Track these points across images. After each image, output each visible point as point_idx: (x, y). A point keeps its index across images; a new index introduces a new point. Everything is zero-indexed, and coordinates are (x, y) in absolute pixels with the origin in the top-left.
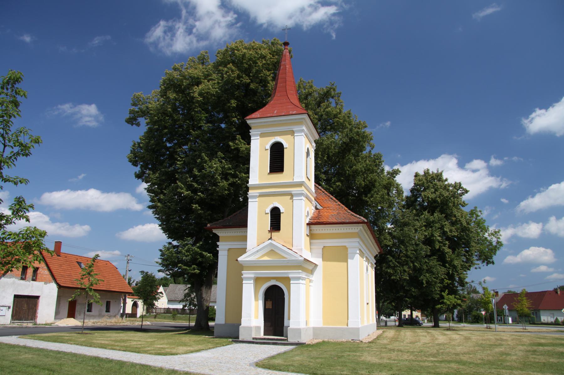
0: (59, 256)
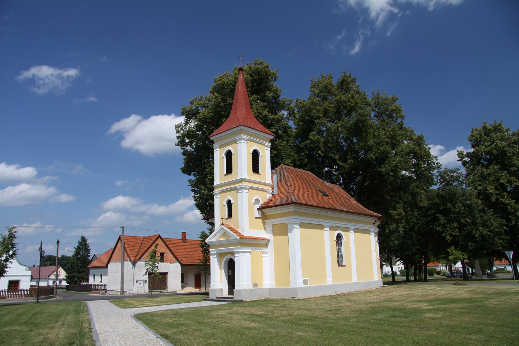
0: (185, 242)
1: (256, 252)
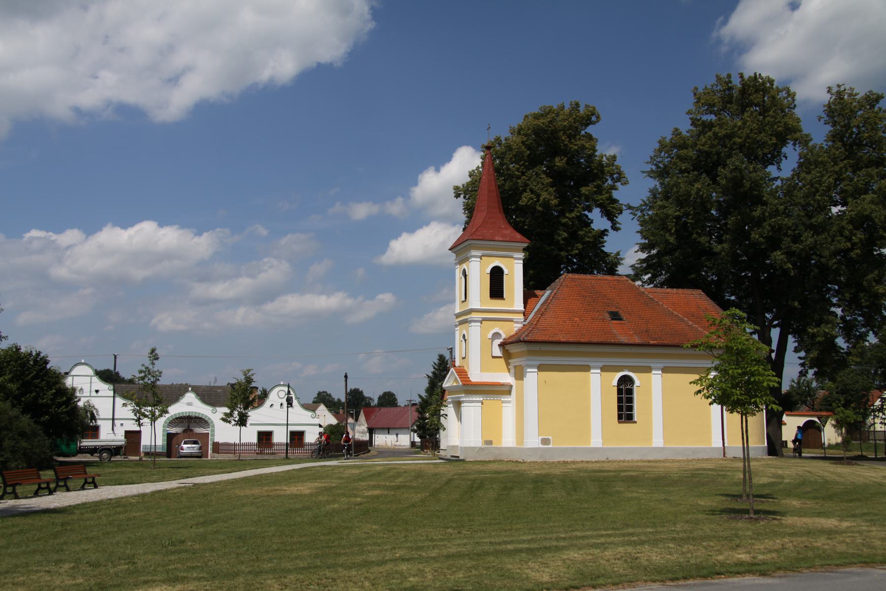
1: (491, 402)
